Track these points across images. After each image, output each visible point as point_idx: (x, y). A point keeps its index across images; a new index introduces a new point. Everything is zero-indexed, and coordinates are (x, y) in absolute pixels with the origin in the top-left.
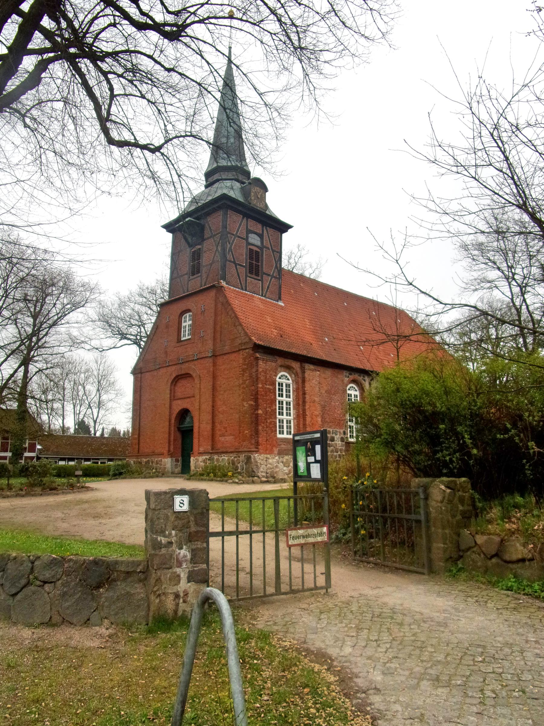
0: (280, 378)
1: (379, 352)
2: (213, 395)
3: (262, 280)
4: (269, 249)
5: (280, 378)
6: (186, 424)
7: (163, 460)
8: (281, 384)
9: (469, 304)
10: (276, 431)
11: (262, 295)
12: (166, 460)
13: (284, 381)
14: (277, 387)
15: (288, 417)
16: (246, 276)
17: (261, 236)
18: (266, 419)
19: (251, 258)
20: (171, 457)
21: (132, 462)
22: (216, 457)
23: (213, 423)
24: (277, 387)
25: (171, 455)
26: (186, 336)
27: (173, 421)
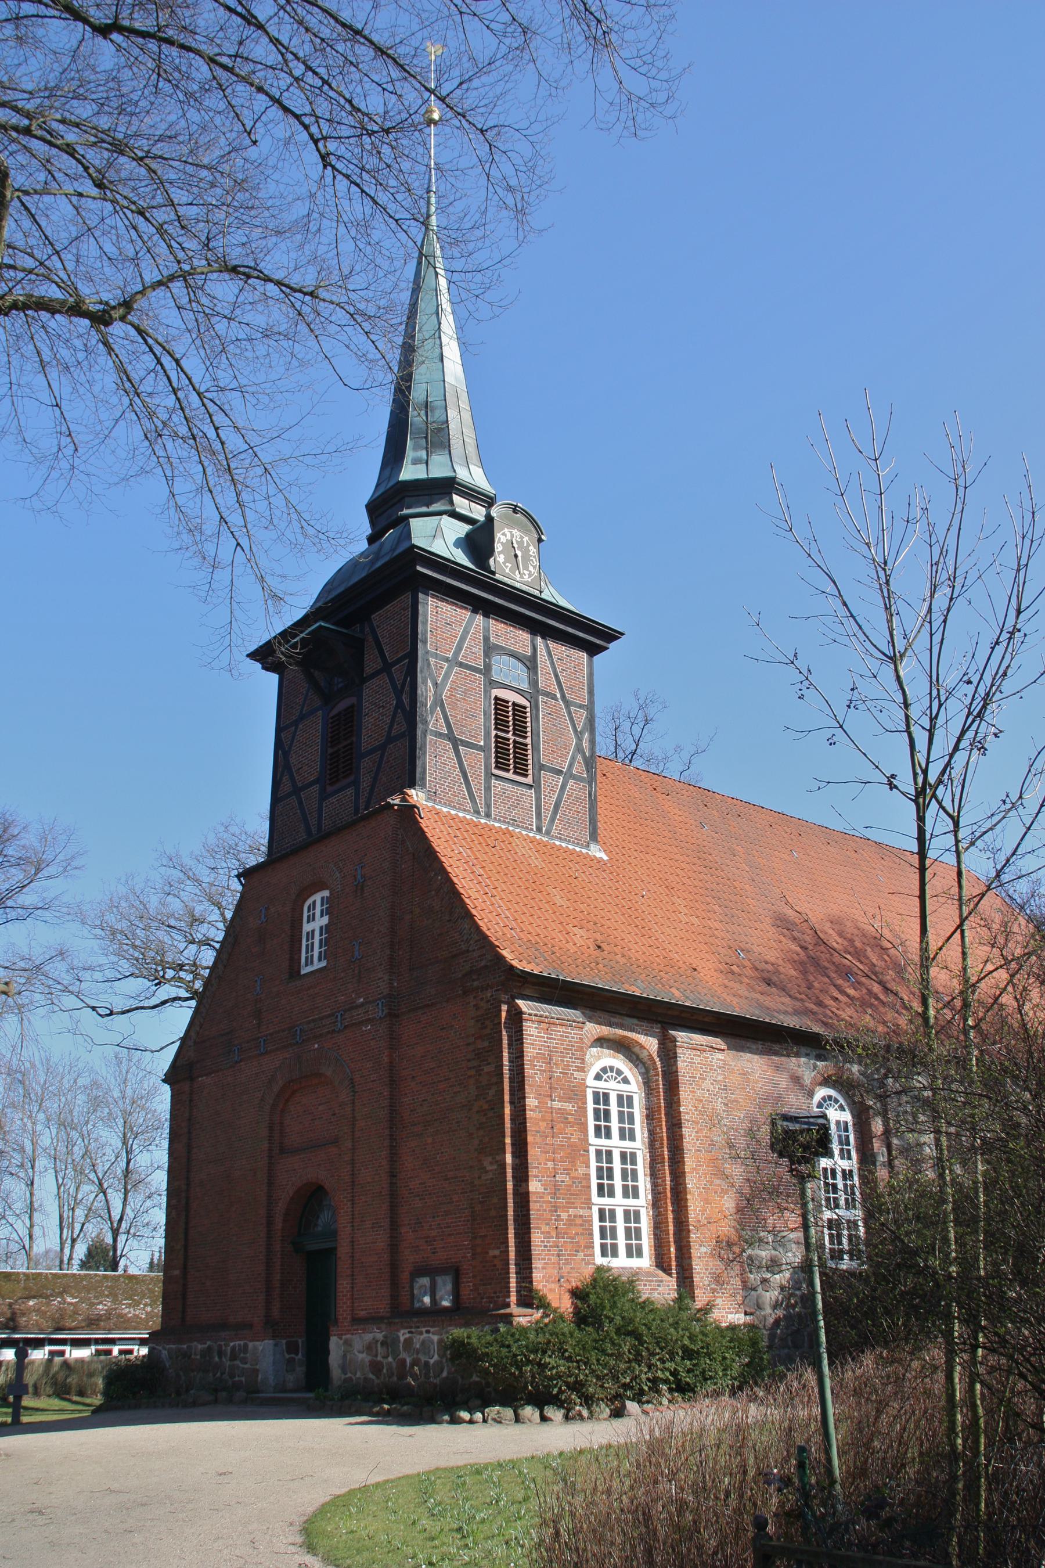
0: (598, 1077)
2: (392, 1137)
3: (536, 786)
4: (554, 697)
5: (598, 1077)
7: (251, 1345)
8: (601, 1098)
10: (591, 1246)
11: (539, 830)
12: (260, 1345)
13: (612, 1087)
14: (590, 1106)
15: (631, 1202)
16: (489, 775)
17: (531, 664)
18: (555, 1209)
19: (500, 723)
20: (274, 1337)
21: (165, 1353)
22: (403, 1335)
23: (394, 1225)
24: (590, 1106)
25: (273, 1328)
26: (313, 960)
27: (279, 1224)
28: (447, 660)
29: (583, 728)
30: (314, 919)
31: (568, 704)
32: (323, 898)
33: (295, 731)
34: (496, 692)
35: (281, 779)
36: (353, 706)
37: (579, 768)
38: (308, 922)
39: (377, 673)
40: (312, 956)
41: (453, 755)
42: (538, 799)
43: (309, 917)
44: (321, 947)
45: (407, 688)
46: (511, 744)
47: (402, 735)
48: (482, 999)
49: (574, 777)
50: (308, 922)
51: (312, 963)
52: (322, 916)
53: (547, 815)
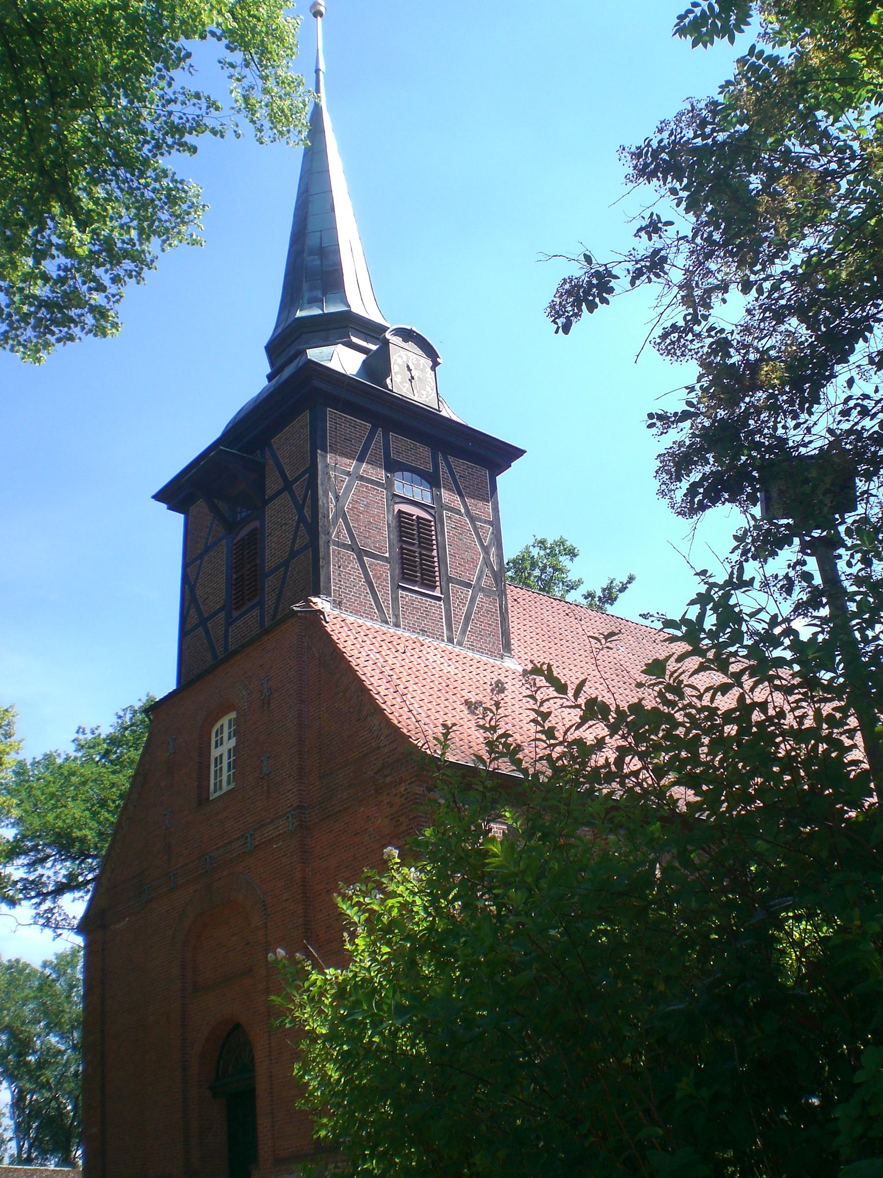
4: (458, 512)
6: (218, 135)
11: (450, 640)
26: (221, 780)
28: (348, 474)
29: (490, 544)
30: (222, 744)
31: (473, 519)
32: (230, 721)
33: (201, 563)
34: (397, 507)
35: (188, 611)
36: (256, 529)
37: (487, 581)
38: (216, 747)
39: (280, 492)
40: (221, 781)
41: (357, 565)
42: (448, 611)
43: (217, 742)
44: (229, 770)
45: (308, 501)
46: (416, 559)
47: (306, 547)
48: (396, 795)
49: (482, 590)
50: (216, 747)
51: (221, 788)
52: (229, 738)
53: (458, 628)
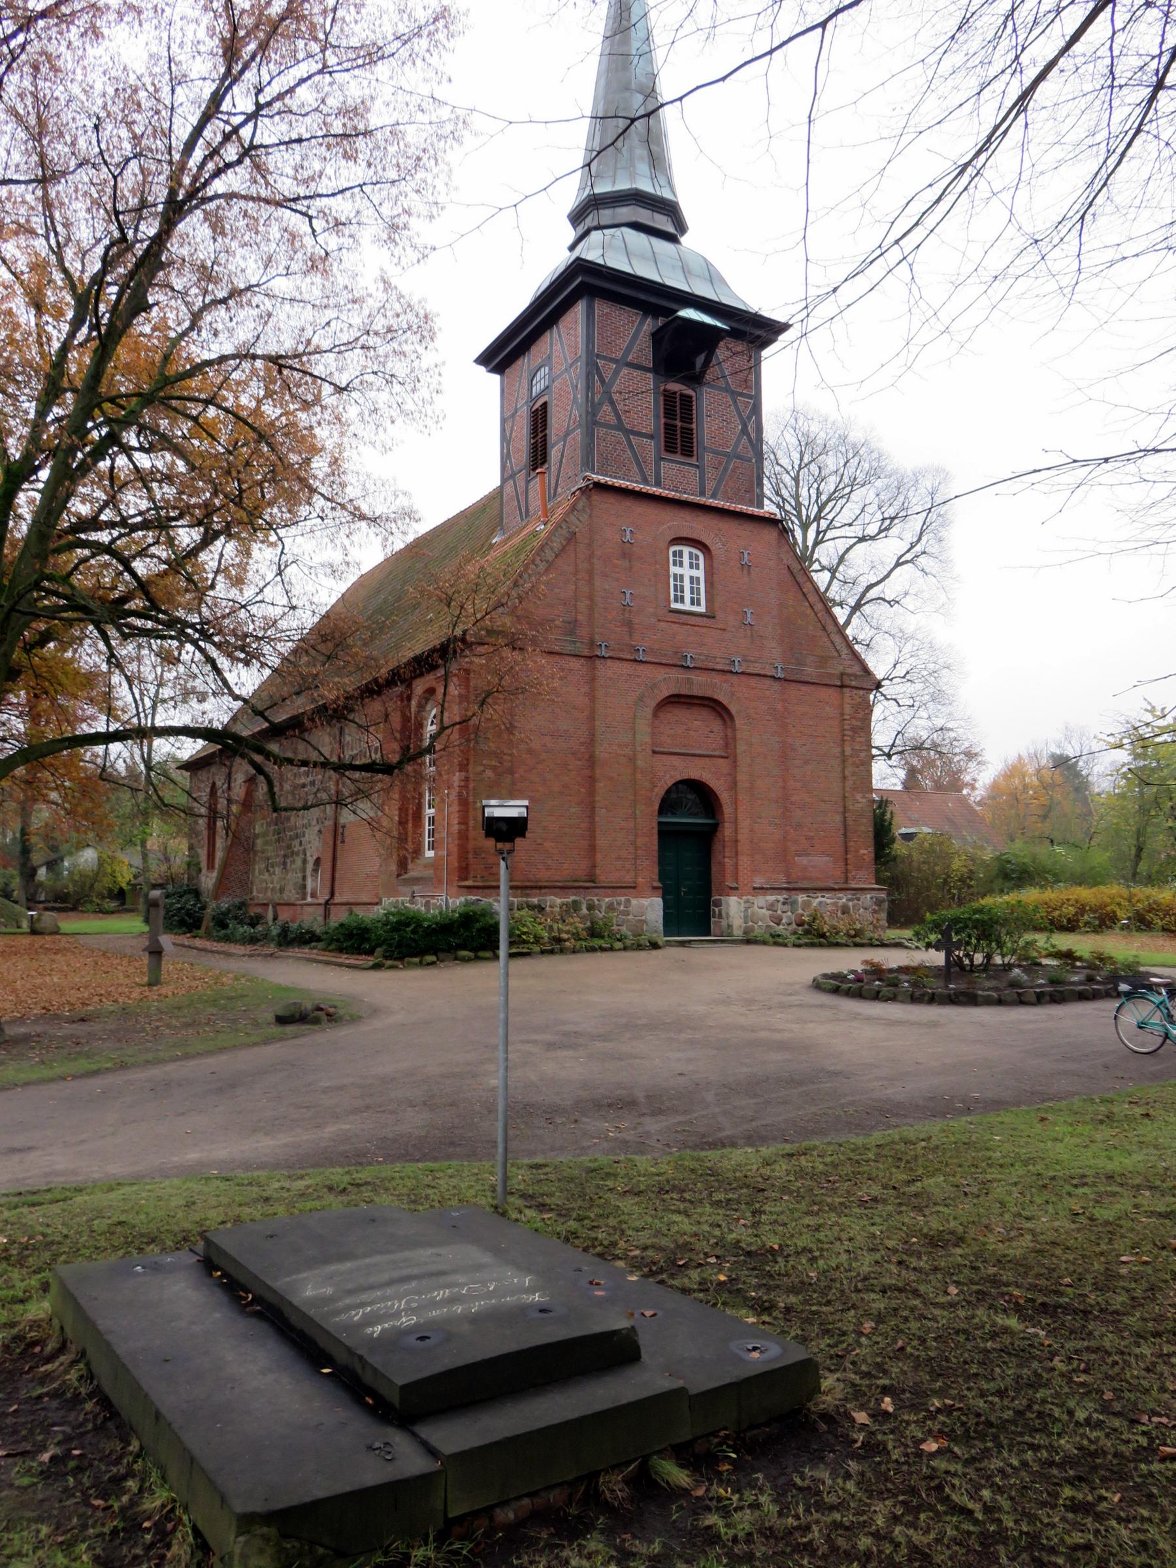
1: (136, 504)
9: (851, 11)
12: (645, 902)
22: (801, 898)
